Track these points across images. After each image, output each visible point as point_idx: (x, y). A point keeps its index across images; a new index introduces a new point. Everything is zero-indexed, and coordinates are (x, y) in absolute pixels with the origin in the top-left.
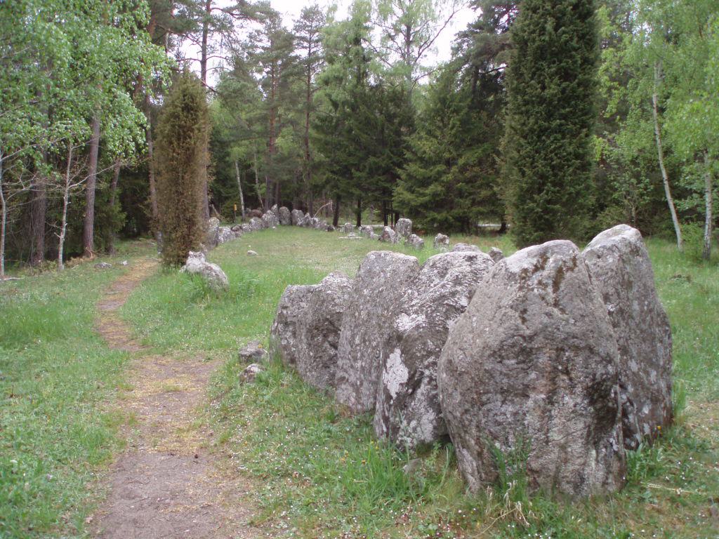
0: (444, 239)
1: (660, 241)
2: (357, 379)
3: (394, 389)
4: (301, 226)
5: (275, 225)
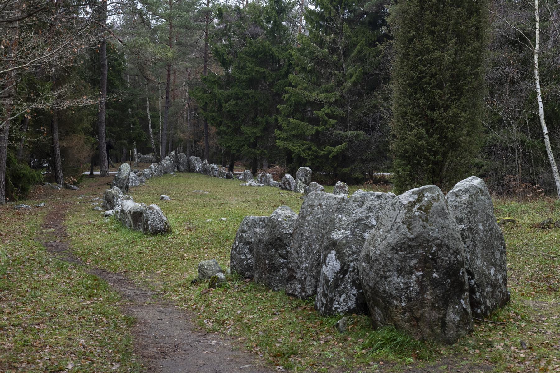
1: (388, 187)
2: (302, 275)
3: (331, 276)
4: (197, 172)
5: (174, 171)
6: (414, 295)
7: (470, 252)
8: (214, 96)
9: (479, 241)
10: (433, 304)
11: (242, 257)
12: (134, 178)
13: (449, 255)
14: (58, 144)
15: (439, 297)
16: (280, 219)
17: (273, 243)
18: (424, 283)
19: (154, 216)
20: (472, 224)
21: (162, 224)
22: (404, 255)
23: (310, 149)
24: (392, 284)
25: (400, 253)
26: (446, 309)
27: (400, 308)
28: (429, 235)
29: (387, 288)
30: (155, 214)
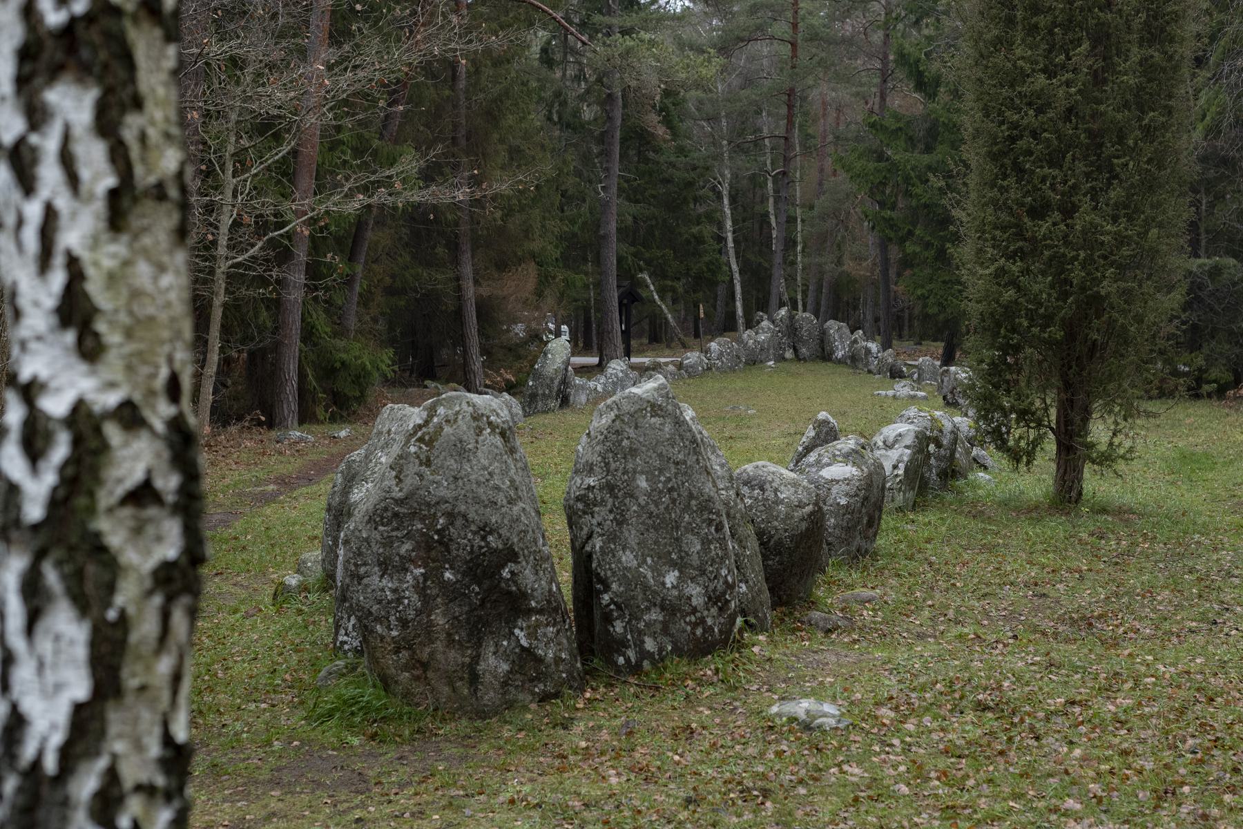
4: (840, 362)
6: (411, 614)
7: (604, 535)
8: (894, 167)
9: (635, 511)
10: (449, 635)
12: (621, 375)
13: (470, 536)
14: (470, 291)
15: (459, 621)
18: (429, 592)
20: (614, 476)
24: (369, 591)
25: (381, 528)
26: (479, 645)
28: (429, 492)
29: (362, 598)
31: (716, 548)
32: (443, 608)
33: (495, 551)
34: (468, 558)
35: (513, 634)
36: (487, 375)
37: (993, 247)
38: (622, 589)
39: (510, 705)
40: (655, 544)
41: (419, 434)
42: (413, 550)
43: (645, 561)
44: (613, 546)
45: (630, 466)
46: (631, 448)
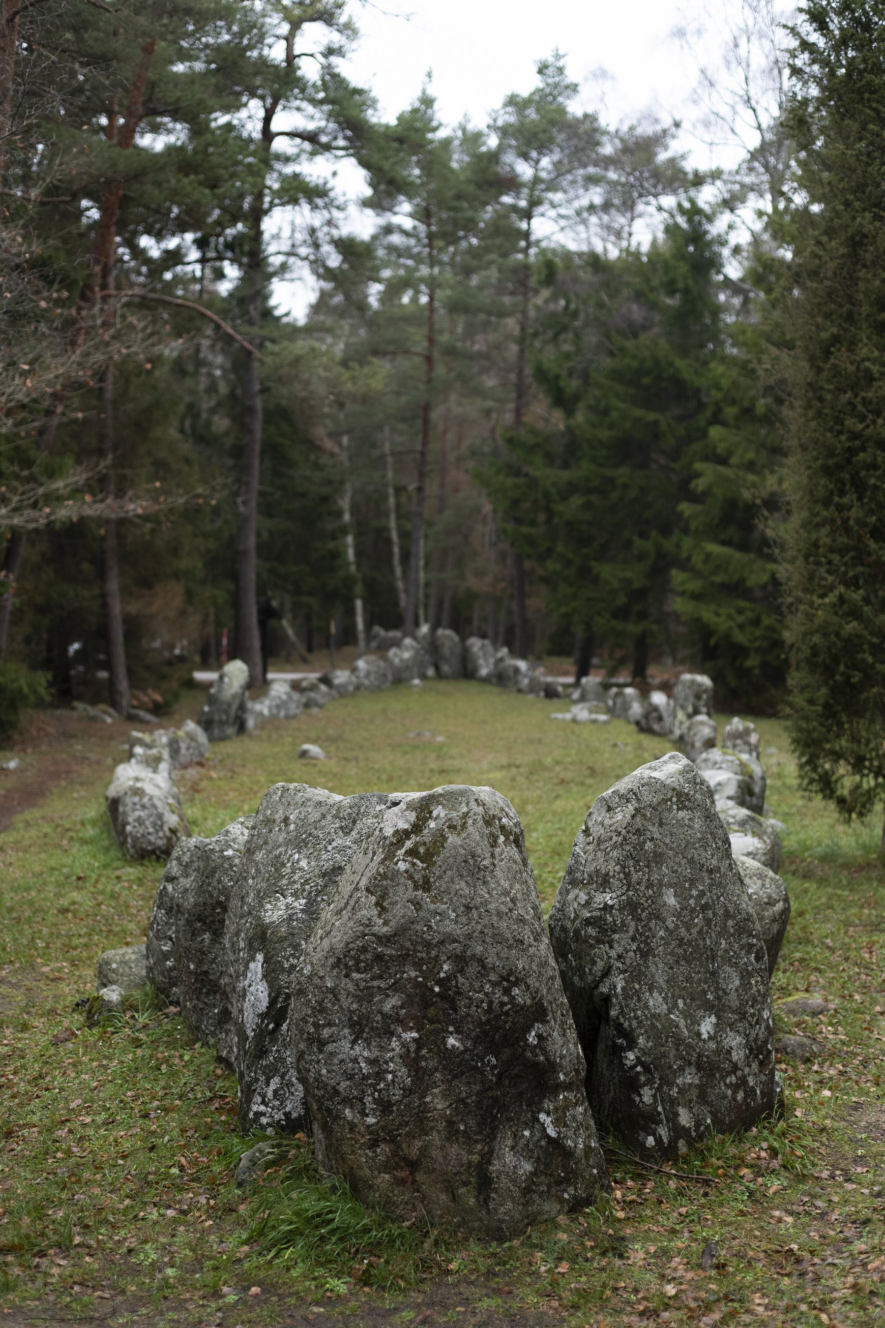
0: (747, 732)
3: (250, 1021)
4: (485, 680)
6: (396, 1094)
7: (625, 971)
8: (533, 483)
9: (662, 938)
10: (450, 1123)
11: (165, 948)
13: (488, 988)
14: (117, 607)
15: (466, 1105)
16: (230, 852)
17: (207, 917)
18: (423, 1064)
19: (142, 814)
20: (636, 890)
21: (161, 834)
22: (367, 982)
23: (756, 622)
24: (336, 1061)
25: (355, 975)
26: (492, 1137)
27: (362, 1129)
28: (430, 927)
29: (324, 1071)
30: (144, 807)
31: (757, 982)
32: (443, 1087)
33: (522, 1008)
34: (484, 1019)
35: (538, 1120)
36: (134, 697)
37: (829, 572)
38: (650, 1044)
39: (533, 1220)
40: (687, 982)
41: (408, 844)
42: (402, 1007)
43: (676, 1005)
44: (637, 987)
45: (655, 877)
46: (655, 852)
